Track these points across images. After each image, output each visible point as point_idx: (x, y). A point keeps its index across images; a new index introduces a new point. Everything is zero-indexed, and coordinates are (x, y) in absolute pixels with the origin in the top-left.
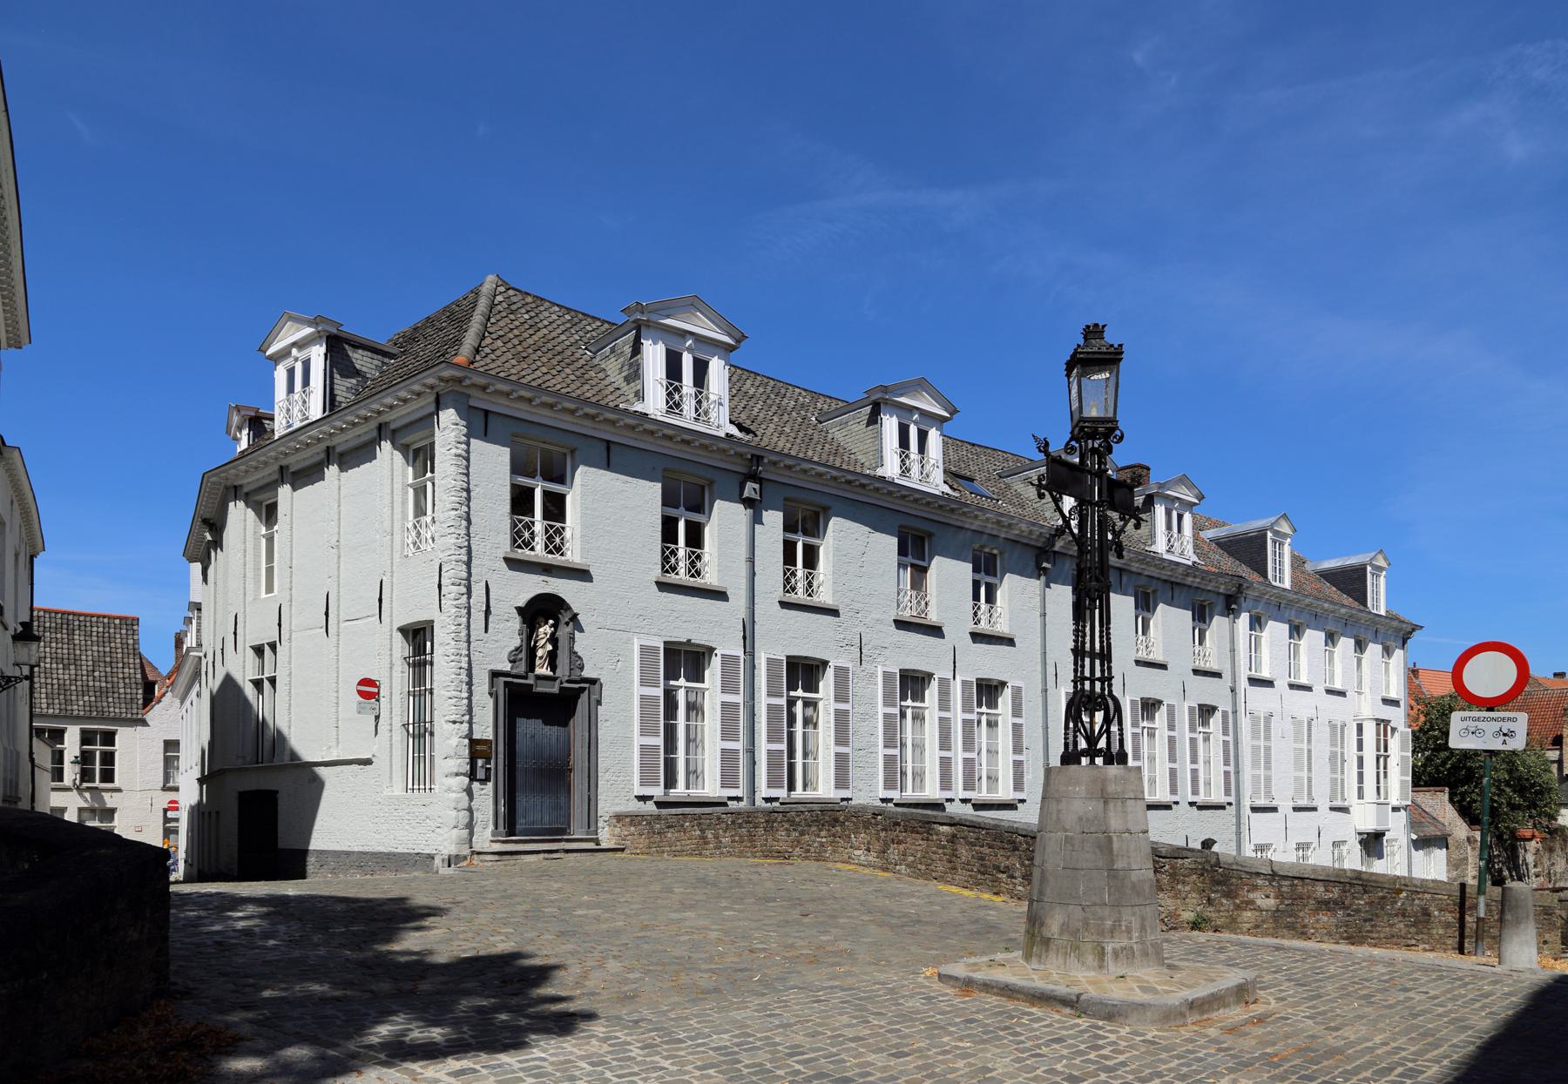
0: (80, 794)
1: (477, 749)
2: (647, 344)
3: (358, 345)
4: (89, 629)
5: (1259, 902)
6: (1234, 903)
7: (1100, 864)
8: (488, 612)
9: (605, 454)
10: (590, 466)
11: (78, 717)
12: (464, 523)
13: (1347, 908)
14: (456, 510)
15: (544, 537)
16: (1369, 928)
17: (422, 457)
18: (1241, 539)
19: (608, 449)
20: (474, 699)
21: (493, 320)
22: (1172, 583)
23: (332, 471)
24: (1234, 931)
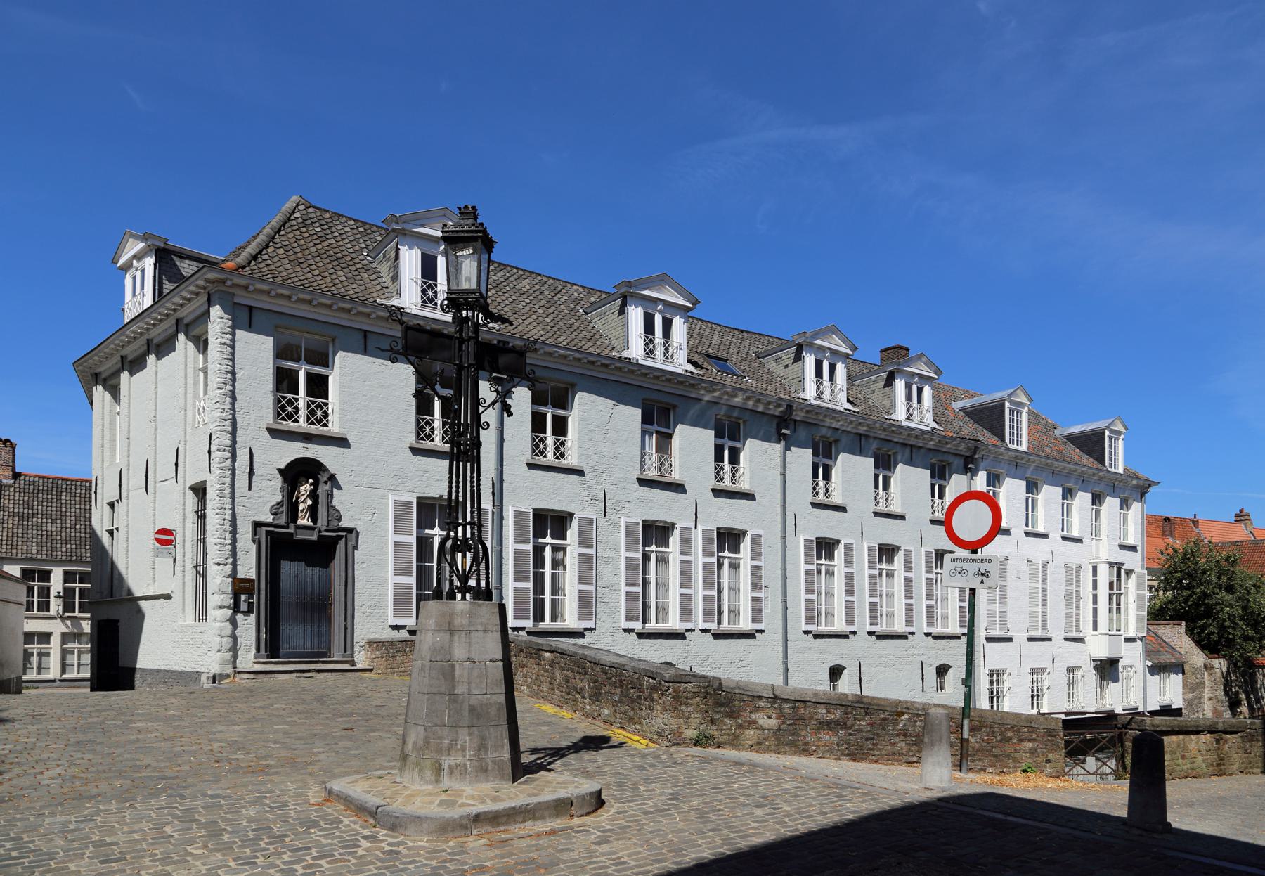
0: (63, 622)
1: (240, 588)
2: (404, 250)
3: (185, 256)
4: (74, 491)
5: (761, 722)
6: (737, 723)
7: (443, 689)
8: (251, 473)
9: (363, 341)
10: (348, 351)
11: (61, 561)
12: (229, 400)
13: (850, 728)
14: (222, 389)
15: (306, 412)
16: (870, 746)
17: (202, 344)
18: (984, 408)
19: (365, 337)
20: (239, 545)
21: (282, 233)
22: (911, 446)
23: (151, 359)
24: (736, 747)
